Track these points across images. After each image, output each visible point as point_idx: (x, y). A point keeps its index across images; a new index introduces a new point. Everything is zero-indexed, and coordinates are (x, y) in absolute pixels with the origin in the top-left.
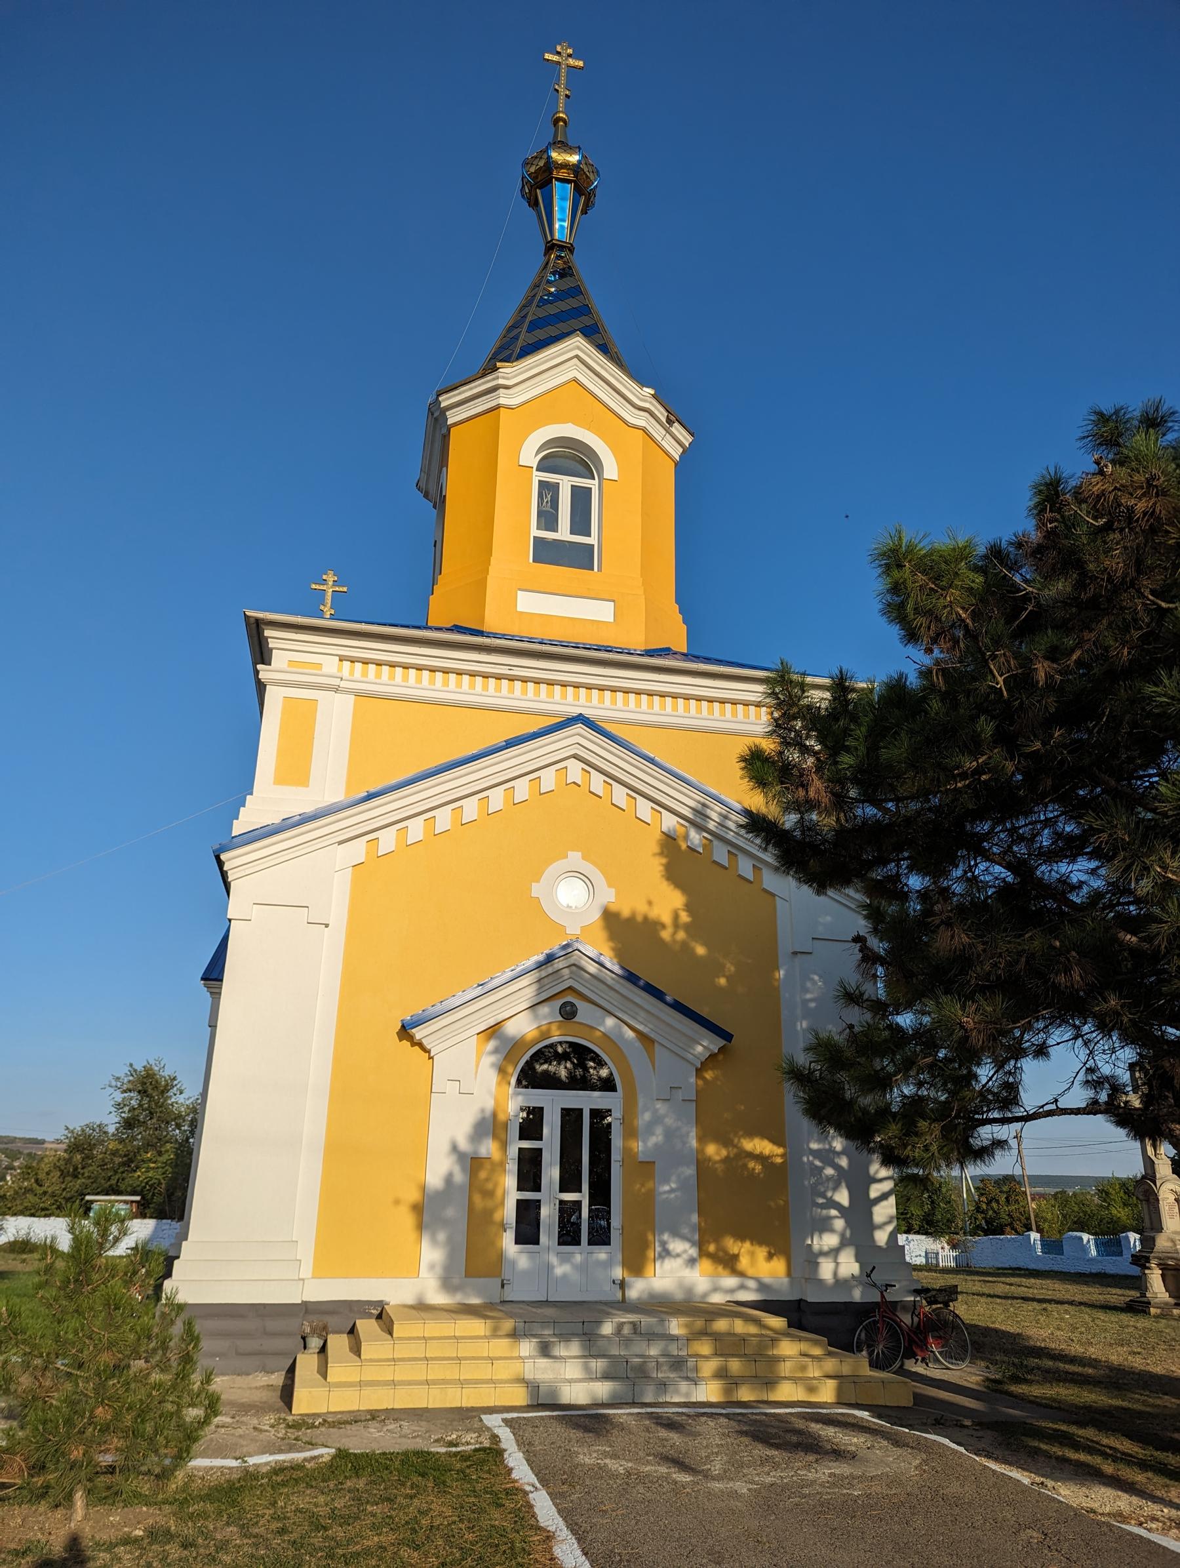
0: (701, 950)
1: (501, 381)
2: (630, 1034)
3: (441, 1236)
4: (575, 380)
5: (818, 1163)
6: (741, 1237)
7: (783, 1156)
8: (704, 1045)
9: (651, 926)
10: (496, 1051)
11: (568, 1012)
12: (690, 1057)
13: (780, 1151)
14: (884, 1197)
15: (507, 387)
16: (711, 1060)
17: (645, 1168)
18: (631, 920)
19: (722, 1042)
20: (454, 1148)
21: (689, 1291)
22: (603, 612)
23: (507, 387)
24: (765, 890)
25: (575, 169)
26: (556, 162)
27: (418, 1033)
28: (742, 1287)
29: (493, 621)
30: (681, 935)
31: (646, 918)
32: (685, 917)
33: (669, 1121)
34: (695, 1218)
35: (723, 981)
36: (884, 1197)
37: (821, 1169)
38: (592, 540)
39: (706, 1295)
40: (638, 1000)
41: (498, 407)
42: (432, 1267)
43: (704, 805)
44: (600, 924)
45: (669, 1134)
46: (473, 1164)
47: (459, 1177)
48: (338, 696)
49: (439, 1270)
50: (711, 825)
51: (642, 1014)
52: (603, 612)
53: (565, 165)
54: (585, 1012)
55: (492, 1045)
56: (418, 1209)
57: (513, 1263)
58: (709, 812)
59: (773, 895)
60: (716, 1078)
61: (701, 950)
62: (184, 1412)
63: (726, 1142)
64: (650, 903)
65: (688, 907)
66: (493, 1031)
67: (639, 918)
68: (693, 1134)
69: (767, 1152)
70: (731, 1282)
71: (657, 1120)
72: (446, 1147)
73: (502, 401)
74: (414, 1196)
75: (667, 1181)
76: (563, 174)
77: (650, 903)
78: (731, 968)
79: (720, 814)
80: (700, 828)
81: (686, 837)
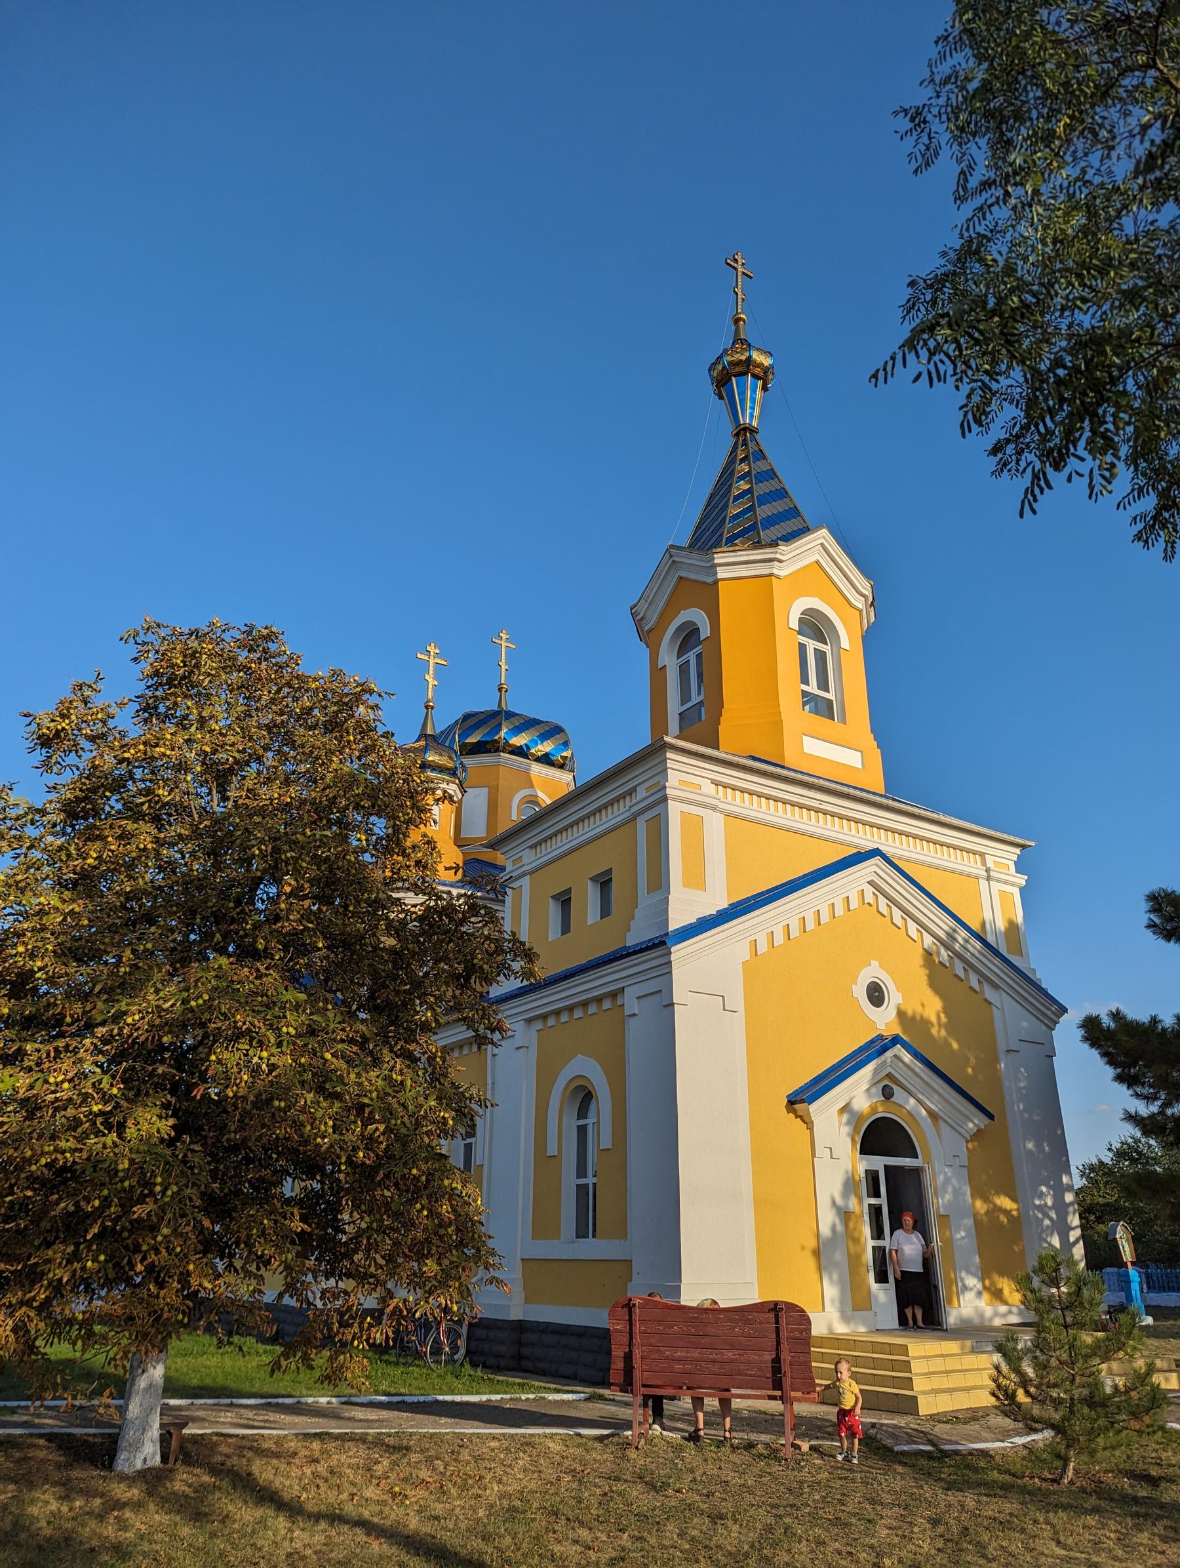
0: (955, 1045)
1: (778, 556)
2: (924, 1112)
3: (835, 1276)
4: (817, 562)
5: (1040, 1216)
6: (1002, 1274)
7: (1018, 1209)
8: (974, 1122)
9: (925, 1023)
10: (848, 1123)
11: (887, 1093)
12: (963, 1132)
13: (1015, 1206)
14: (1076, 1242)
15: (780, 561)
16: (978, 1135)
17: (944, 1218)
18: (913, 1018)
19: (987, 1121)
20: (834, 1203)
21: (981, 1315)
22: (852, 759)
23: (780, 561)
24: (986, 1000)
25: (766, 370)
26: (755, 361)
27: (796, 1106)
28: (1010, 1312)
29: (790, 760)
30: (943, 1033)
31: (922, 1017)
32: (944, 1019)
33: (954, 1181)
34: (977, 1259)
35: (970, 1070)
36: (1076, 1242)
37: (1042, 1220)
38: (830, 696)
39: (991, 1320)
40: (936, 1087)
41: (771, 575)
42: (832, 1301)
43: (954, 931)
44: (896, 1021)
45: (956, 1193)
46: (845, 1215)
47: (840, 1228)
48: (715, 814)
49: (837, 1303)
50: (957, 946)
51: (936, 1096)
52: (852, 759)
53: (760, 365)
54: (898, 1093)
55: (845, 1117)
56: (817, 1253)
57: (876, 1297)
58: (956, 936)
59: (990, 1003)
60: (974, 1148)
61: (955, 1045)
62: (47, 1532)
63: (986, 1200)
64: (923, 1005)
65: (946, 1010)
66: (846, 1109)
67: (918, 1018)
68: (969, 1193)
69: (1008, 1208)
70: (1003, 1309)
71: (947, 1181)
72: (829, 1203)
73: (775, 571)
74: (812, 1243)
75: (958, 1231)
76: (757, 371)
77: (923, 1005)
78: (973, 1061)
79: (964, 939)
80: (947, 947)
81: (938, 953)
